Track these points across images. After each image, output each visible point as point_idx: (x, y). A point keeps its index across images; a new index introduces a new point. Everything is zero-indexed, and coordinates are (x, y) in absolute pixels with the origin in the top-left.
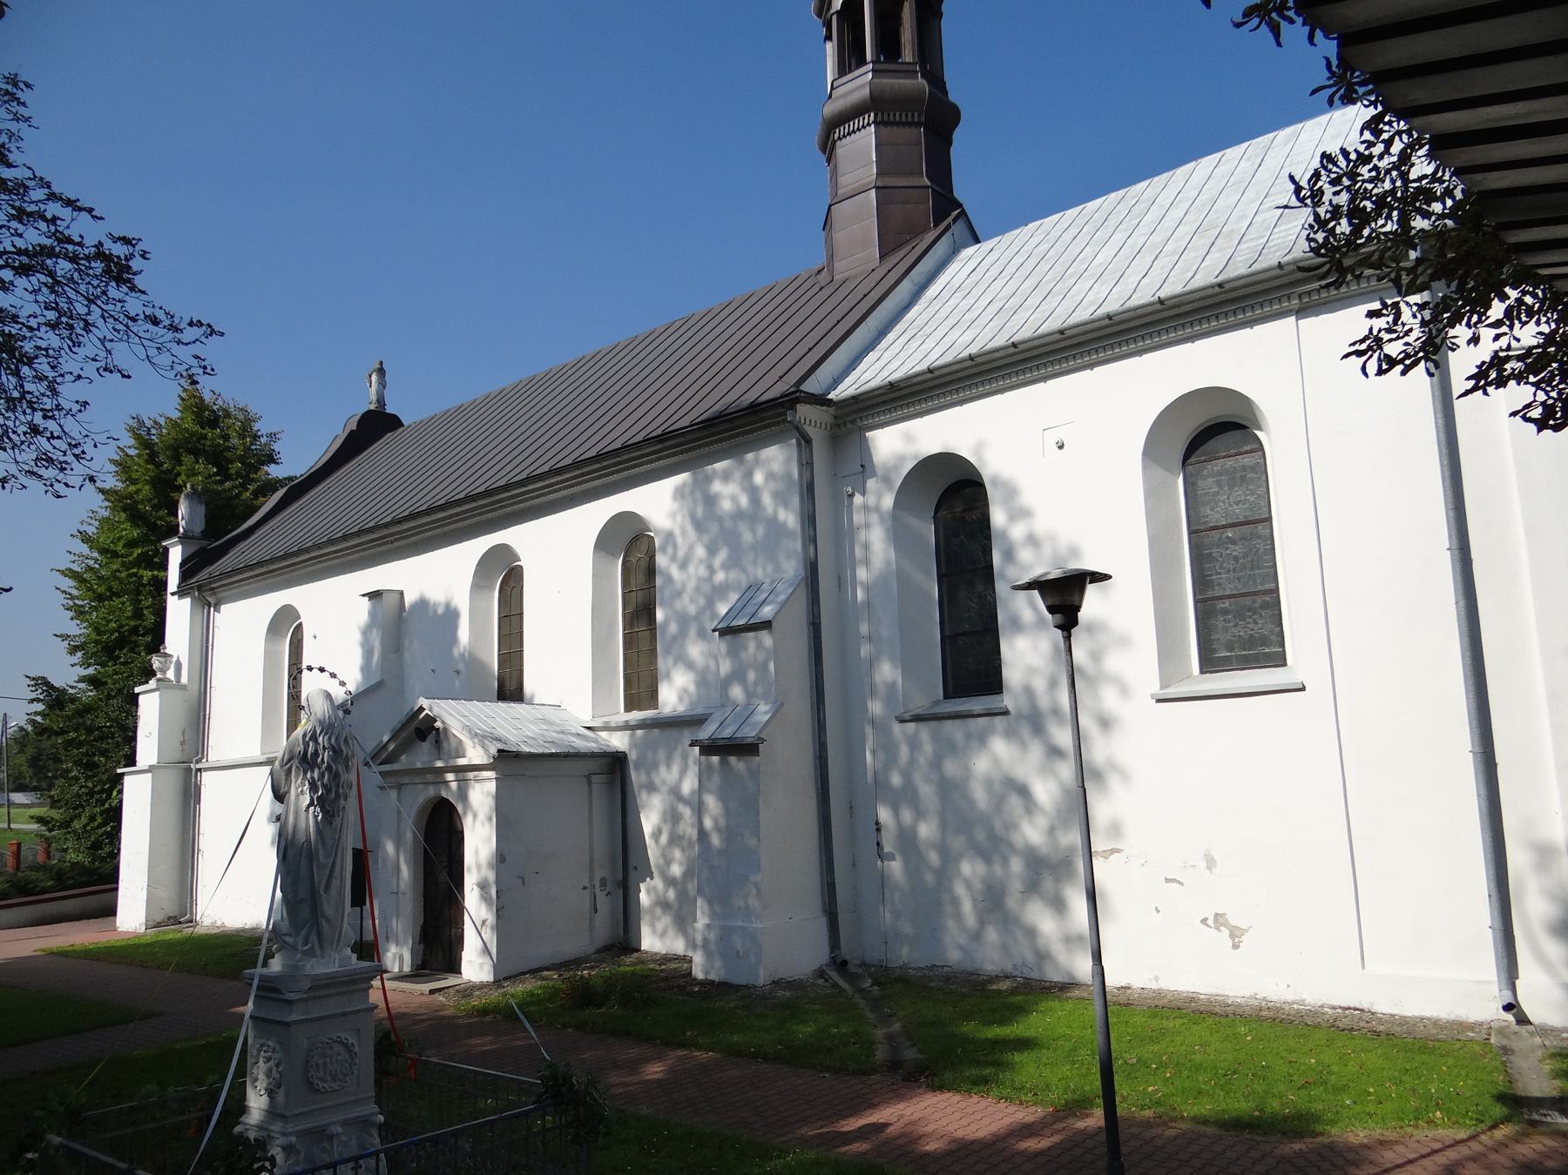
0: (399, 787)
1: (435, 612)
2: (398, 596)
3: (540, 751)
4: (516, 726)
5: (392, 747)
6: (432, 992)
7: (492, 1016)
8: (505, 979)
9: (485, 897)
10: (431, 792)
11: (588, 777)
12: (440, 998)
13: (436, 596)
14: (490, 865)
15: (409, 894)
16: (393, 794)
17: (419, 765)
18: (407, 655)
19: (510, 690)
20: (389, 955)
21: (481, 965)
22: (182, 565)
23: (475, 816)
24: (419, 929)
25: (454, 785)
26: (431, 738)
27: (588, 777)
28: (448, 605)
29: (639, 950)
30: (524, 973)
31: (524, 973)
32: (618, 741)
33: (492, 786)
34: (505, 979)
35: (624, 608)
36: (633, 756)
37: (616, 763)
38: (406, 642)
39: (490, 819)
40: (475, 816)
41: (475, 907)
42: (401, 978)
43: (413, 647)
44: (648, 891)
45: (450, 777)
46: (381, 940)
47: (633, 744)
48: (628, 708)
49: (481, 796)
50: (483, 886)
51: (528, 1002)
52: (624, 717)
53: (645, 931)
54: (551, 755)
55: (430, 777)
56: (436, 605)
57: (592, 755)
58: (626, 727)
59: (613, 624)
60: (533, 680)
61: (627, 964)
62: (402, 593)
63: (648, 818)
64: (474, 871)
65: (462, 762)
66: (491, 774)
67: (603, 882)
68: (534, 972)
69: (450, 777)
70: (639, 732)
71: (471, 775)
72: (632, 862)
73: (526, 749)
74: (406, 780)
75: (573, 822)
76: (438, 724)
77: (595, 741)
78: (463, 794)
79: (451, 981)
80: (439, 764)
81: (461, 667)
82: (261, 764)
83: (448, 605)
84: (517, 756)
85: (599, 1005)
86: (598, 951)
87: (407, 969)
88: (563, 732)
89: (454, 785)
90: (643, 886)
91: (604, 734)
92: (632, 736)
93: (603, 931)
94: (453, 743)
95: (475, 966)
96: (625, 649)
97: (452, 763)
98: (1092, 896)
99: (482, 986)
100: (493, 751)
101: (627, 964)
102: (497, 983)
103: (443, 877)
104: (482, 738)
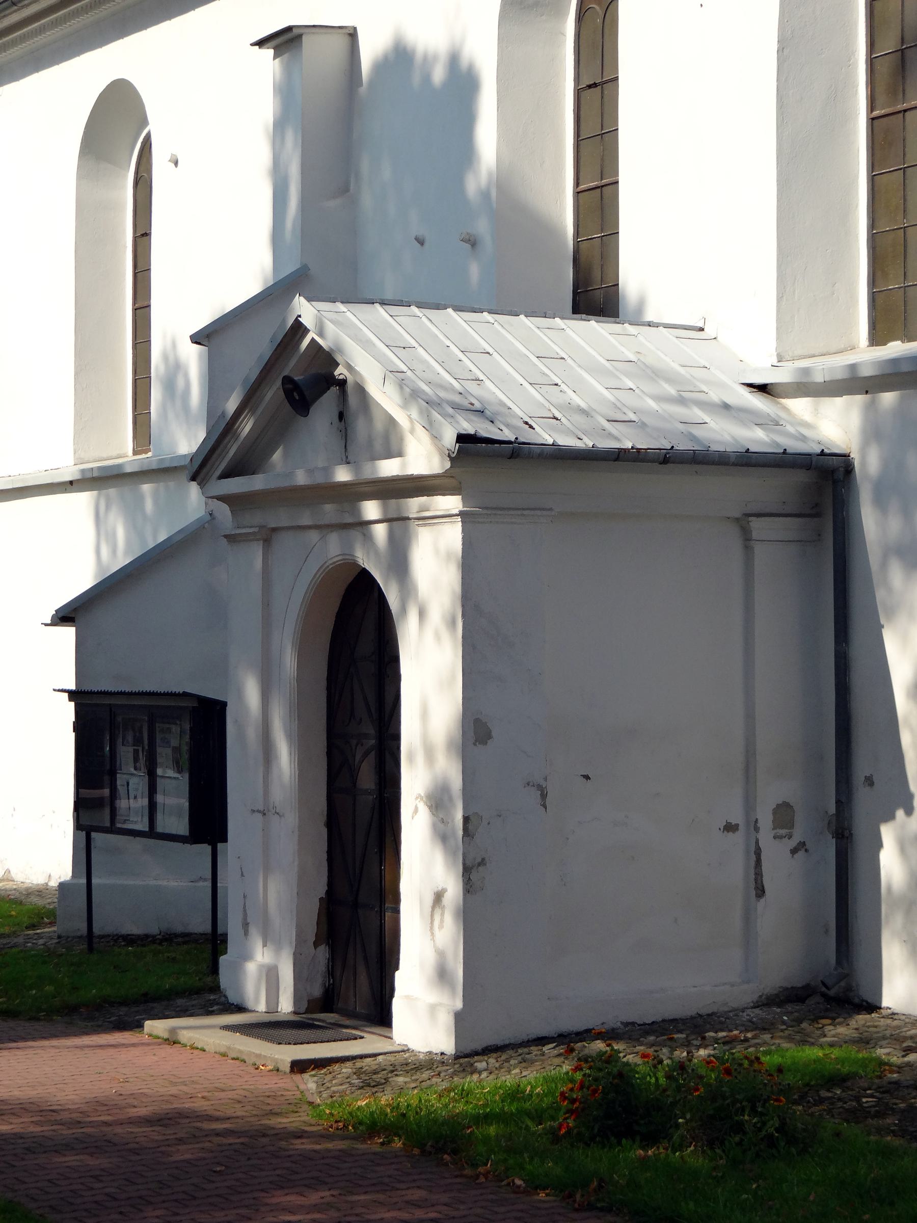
0: (268, 536)
1: (427, 78)
2: (340, 43)
3: (587, 443)
4: (553, 378)
5: (247, 427)
6: (299, 1067)
7: (428, 1144)
8: (487, 1051)
9: (442, 835)
10: (333, 548)
11: (743, 523)
12: (309, 1083)
13: (429, 38)
14: (450, 745)
15: (291, 819)
16: (256, 553)
17: (301, 478)
18: (367, 200)
19: (594, 294)
20: (251, 968)
21: (433, 1009)
22: (909, 341)
23: (422, 614)
24: (314, 907)
25: (380, 531)
26: (323, 410)
27: (743, 523)
28: (454, 59)
29: (873, 1007)
30: (541, 1041)
31: (541, 1041)
32: (833, 425)
33: (452, 535)
34: (487, 1051)
35: (872, 45)
36: (869, 464)
37: (824, 482)
38: (365, 165)
39: (452, 623)
40: (422, 614)
41: (424, 868)
42: (270, 1028)
43: (382, 178)
44: (903, 848)
45: (371, 510)
46: (232, 926)
47: (873, 431)
48: (877, 337)
49: (432, 566)
50: (437, 801)
51: (515, 1110)
52: (867, 355)
53: (893, 956)
54: (619, 456)
55: (330, 511)
56: (428, 61)
57: (747, 461)
58: (853, 383)
59: (843, 88)
60: (637, 268)
61: (830, 1044)
62: (352, 34)
63: (905, 639)
64: (420, 759)
65: (389, 468)
66: (451, 503)
67: (784, 815)
68: (567, 1040)
69: (371, 510)
70: (888, 398)
71: (414, 505)
72: (862, 767)
73: (545, 436)
74: (280, 517)
75: (697, 649)
76: (340, 372)
77: (773, 424)
78: (399, 560)
79: (369, 1043)
80: (343, 475)
81: (482, 227)
82: (70, 486)
83: (454, 59)
84: (517, 453)
85: (650, 1140)
86: (768, 1002)
87: (286, 1006)
88: (681, 401)
89: (380, 531)
90: (888, 833)
91: (800, 407)
92: (870, 409)
93: (781, 951)
94: (379, 425)
95: (422, 1016)
96: (872, 164)
97: (367, 473)
98: (299, 1136)
99: (431, 1063)
100: (449, 438)
101: (830, 1044)
102: (465, 1058)
103: (367, 779)
104: (431, 405)
